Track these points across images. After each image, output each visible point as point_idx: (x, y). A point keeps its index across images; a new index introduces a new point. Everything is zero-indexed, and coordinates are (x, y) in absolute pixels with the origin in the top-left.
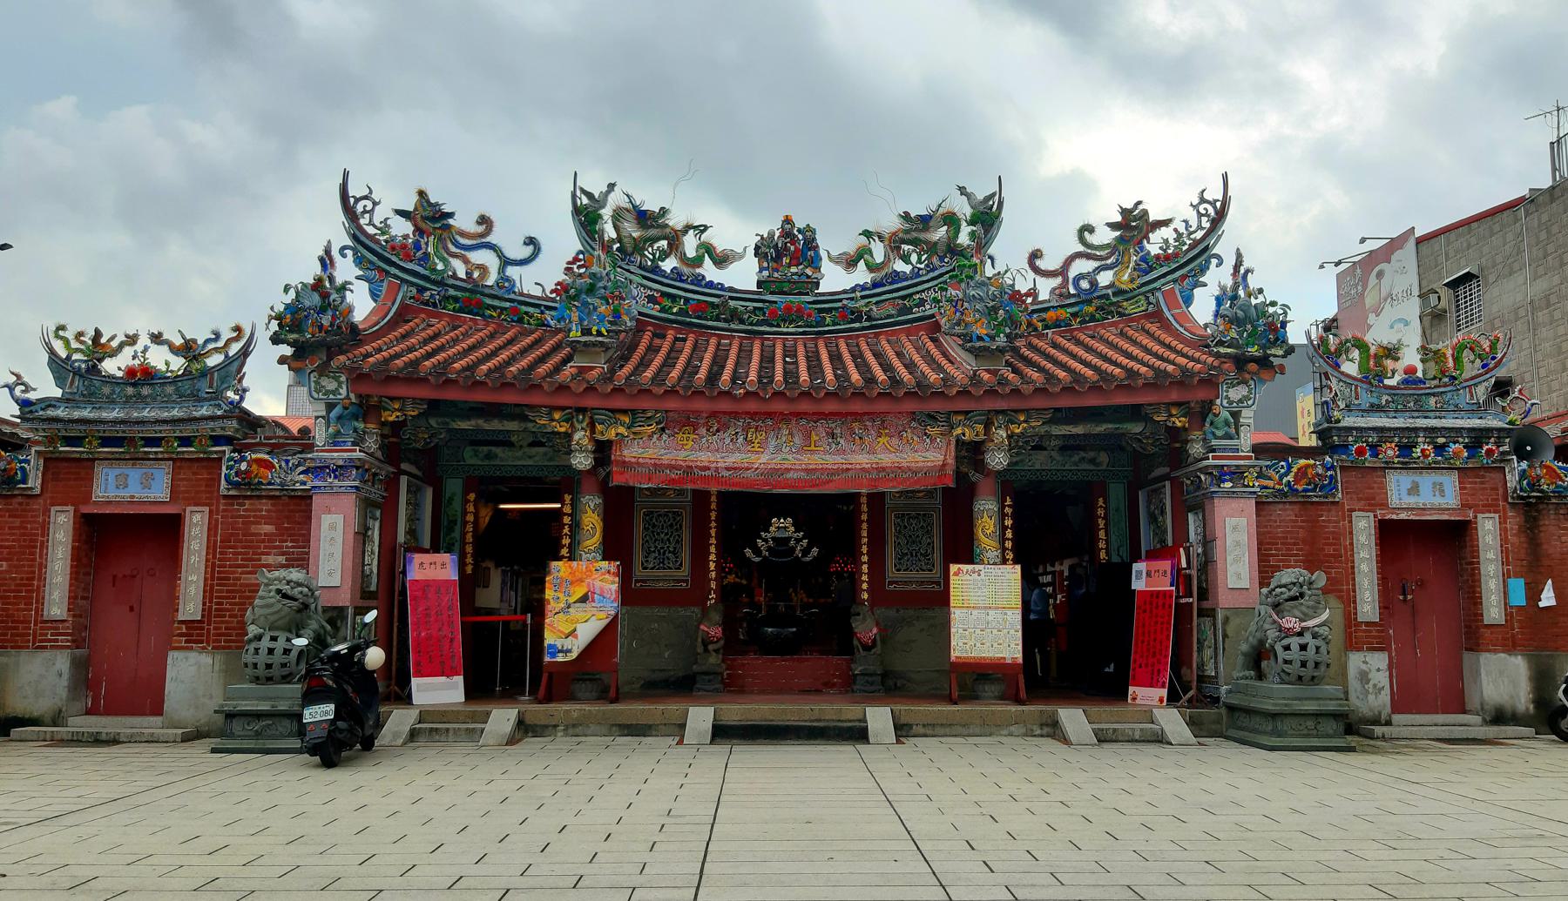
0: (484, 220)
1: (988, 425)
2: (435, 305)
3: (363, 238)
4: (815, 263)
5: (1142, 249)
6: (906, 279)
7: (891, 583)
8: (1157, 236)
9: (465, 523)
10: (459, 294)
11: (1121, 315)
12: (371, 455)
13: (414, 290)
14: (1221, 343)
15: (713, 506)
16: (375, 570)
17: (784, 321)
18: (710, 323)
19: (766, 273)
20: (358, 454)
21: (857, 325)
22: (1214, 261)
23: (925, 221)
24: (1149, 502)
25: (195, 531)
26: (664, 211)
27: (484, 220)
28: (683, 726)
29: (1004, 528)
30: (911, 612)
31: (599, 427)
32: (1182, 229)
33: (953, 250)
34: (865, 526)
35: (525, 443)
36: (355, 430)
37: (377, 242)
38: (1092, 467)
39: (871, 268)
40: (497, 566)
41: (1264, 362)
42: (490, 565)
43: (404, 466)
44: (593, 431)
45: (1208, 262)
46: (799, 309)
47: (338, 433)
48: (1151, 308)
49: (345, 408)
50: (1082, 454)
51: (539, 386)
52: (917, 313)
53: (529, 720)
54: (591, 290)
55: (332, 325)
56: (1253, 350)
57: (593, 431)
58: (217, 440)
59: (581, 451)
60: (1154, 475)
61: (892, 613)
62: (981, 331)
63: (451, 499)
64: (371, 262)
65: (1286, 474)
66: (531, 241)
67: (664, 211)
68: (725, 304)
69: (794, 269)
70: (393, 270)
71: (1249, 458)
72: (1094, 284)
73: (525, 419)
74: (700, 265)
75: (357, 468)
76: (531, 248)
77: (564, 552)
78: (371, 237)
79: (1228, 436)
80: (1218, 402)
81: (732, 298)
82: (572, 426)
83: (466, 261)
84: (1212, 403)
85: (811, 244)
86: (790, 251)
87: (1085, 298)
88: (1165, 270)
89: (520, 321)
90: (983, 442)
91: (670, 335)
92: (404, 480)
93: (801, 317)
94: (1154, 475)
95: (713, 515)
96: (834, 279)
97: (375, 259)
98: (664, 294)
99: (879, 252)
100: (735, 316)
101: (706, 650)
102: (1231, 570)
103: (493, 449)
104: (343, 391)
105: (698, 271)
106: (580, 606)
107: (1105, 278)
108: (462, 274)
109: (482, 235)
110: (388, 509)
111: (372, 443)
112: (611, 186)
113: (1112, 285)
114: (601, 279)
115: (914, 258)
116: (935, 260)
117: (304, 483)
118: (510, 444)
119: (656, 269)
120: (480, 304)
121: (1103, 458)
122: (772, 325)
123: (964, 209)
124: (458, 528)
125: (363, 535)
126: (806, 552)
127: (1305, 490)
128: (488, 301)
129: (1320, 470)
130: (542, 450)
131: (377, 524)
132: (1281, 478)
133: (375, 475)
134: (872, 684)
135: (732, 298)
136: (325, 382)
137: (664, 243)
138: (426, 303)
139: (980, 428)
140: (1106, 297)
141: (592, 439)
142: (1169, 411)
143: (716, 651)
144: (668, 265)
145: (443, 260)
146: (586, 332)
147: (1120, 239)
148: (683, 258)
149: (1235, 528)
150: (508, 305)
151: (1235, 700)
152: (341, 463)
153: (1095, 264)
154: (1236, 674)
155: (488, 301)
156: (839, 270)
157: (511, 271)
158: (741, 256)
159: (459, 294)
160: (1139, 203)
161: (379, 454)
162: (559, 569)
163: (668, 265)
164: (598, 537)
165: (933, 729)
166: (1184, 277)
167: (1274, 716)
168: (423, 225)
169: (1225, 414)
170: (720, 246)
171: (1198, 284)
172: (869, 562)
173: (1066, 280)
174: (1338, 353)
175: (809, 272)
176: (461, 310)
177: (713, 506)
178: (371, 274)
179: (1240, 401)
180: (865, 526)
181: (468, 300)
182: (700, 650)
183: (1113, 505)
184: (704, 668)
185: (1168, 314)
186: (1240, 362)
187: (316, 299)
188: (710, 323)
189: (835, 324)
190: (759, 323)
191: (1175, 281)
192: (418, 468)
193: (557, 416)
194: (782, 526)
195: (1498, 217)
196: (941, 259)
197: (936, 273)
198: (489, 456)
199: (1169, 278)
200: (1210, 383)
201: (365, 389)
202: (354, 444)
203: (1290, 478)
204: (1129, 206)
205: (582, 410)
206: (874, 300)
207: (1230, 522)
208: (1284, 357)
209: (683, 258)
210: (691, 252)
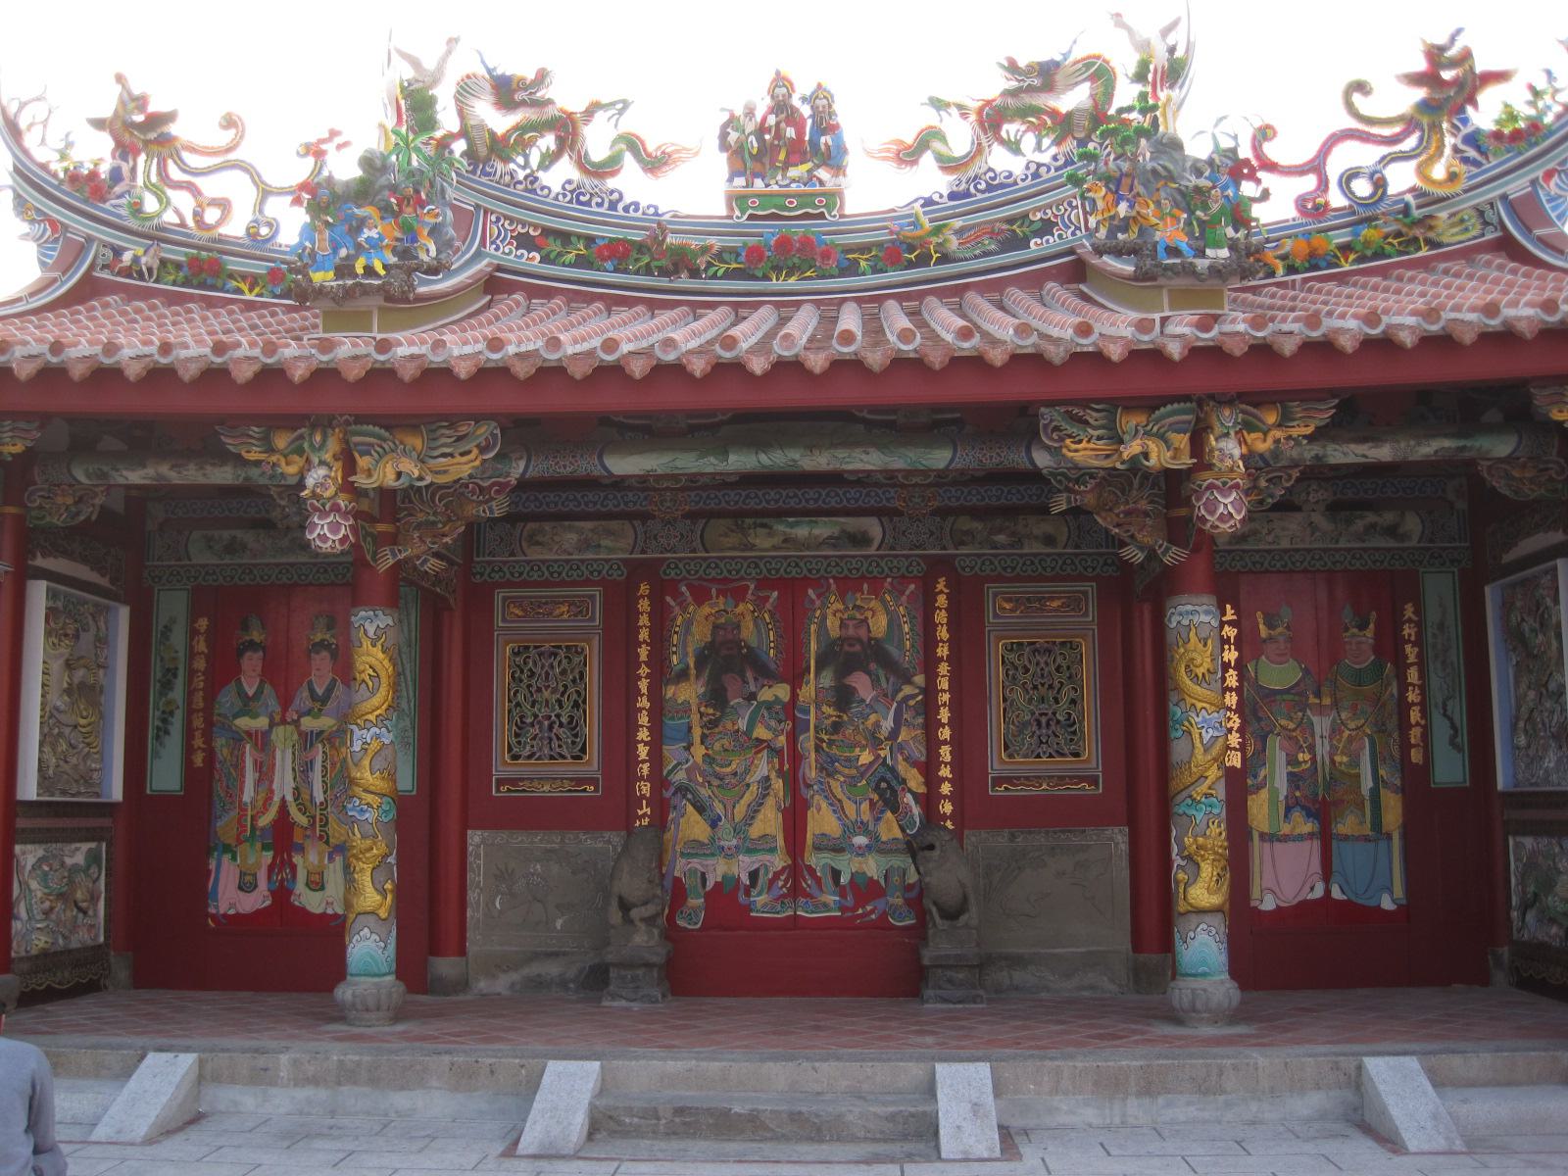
4: (834, 159)
5: (1465, 121)
7: (998, 781)
11: (1432, 244)
17: (777, 269)
23: (1047, 75)
24: (1507, 607)
26: (542, 77)
31: (363, 462)
38: (1392, 544)
39: (948, 165)
50: (1371, 517)
61: (1001, 840)
63: (167, 629)
67: (542, 77)
72: (1380, 184)
85: (825, 123)
87: (1362, 214)
98: (547, 232)
99: (960, 137)
103: (239, 534)
107: (1401, 179)
109: (229, 150)
112: (452, 42)
122: (754, 278)
123: (1124, 63)
137: (548, 141)
138: (127, 272)
139: (1182, 440)
141: (348, 487)
143: (650, 921)
147: (1425, 106)
160: (1459, 31)
168: (127, 138)
172: (953, 742)
173: (1323, 184)
182: (616, 916)
183: (1433, 615)
192: (97, 566)
193: (281, 441)
198: (232, 548)
204: (1441, 39)
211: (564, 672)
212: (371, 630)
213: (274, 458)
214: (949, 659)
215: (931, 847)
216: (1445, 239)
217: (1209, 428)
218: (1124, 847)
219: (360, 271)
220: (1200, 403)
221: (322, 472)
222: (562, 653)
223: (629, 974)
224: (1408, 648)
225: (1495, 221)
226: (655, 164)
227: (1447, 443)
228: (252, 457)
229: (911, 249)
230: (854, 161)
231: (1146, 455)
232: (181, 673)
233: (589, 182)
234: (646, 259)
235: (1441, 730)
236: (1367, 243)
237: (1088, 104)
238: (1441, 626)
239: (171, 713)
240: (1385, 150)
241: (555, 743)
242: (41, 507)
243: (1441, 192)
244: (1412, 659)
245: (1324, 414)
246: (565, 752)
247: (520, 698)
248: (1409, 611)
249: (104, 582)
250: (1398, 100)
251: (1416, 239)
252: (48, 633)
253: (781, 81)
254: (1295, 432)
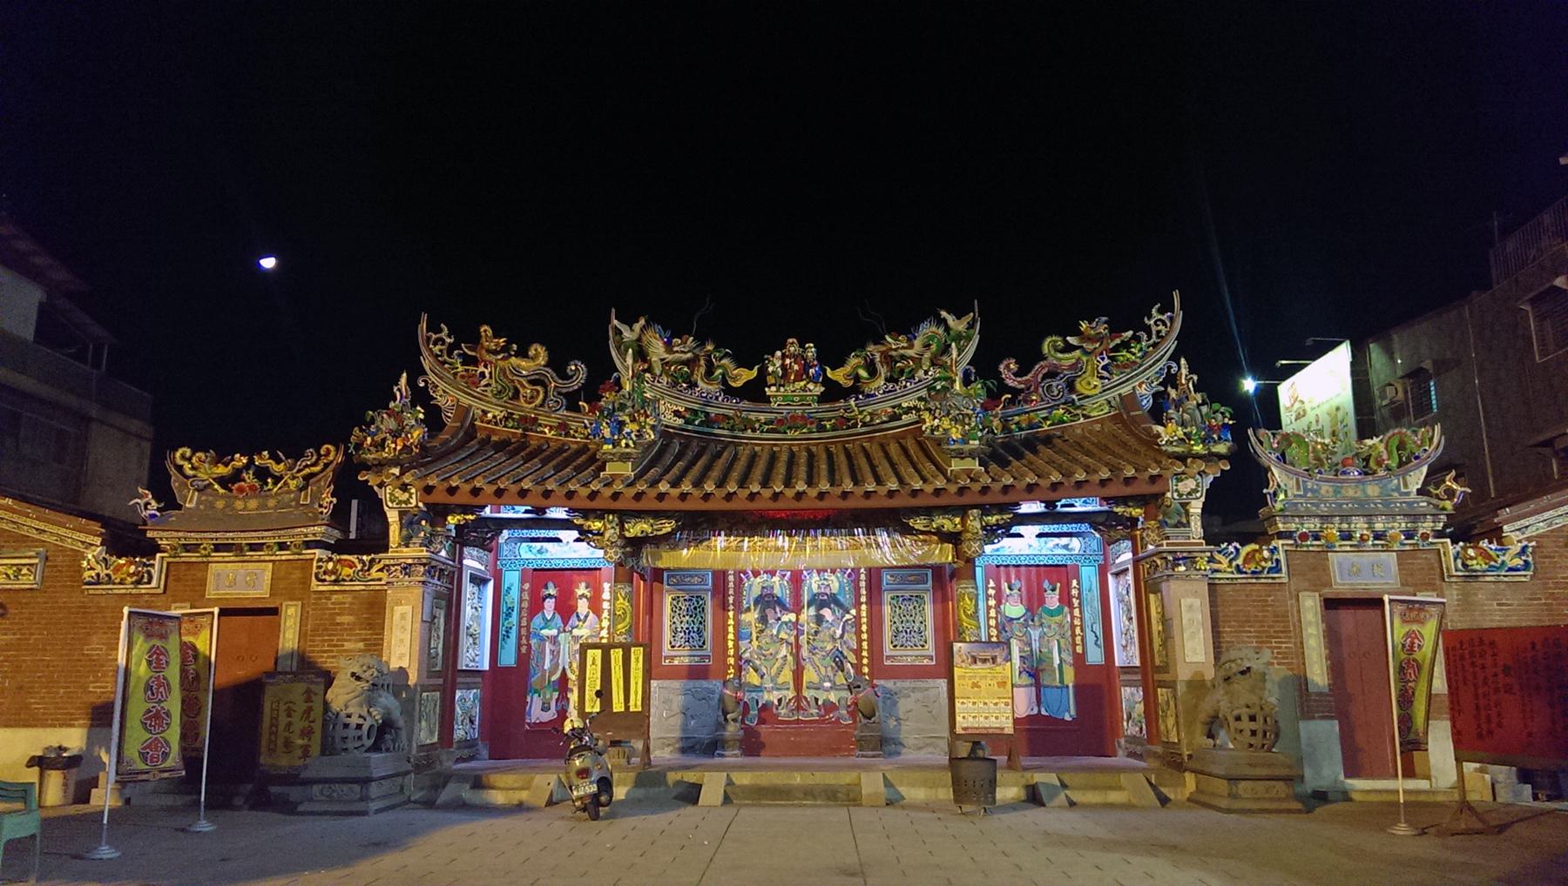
7: (888, 657)
25: (290, 622)
29: (1079, 597)
30: (458, 709)
58: (308, 545)
80: (1169, 495)
90: (960, 533)
102: (1188, 645)
104: (413, 501)
124: (515, 614)
138: (489, 422)
139: (958, 520)
143: (735, 720)
149: (1190, 607)
198: (540, 552)
203: (1240, 561)
207: (1185, 602)
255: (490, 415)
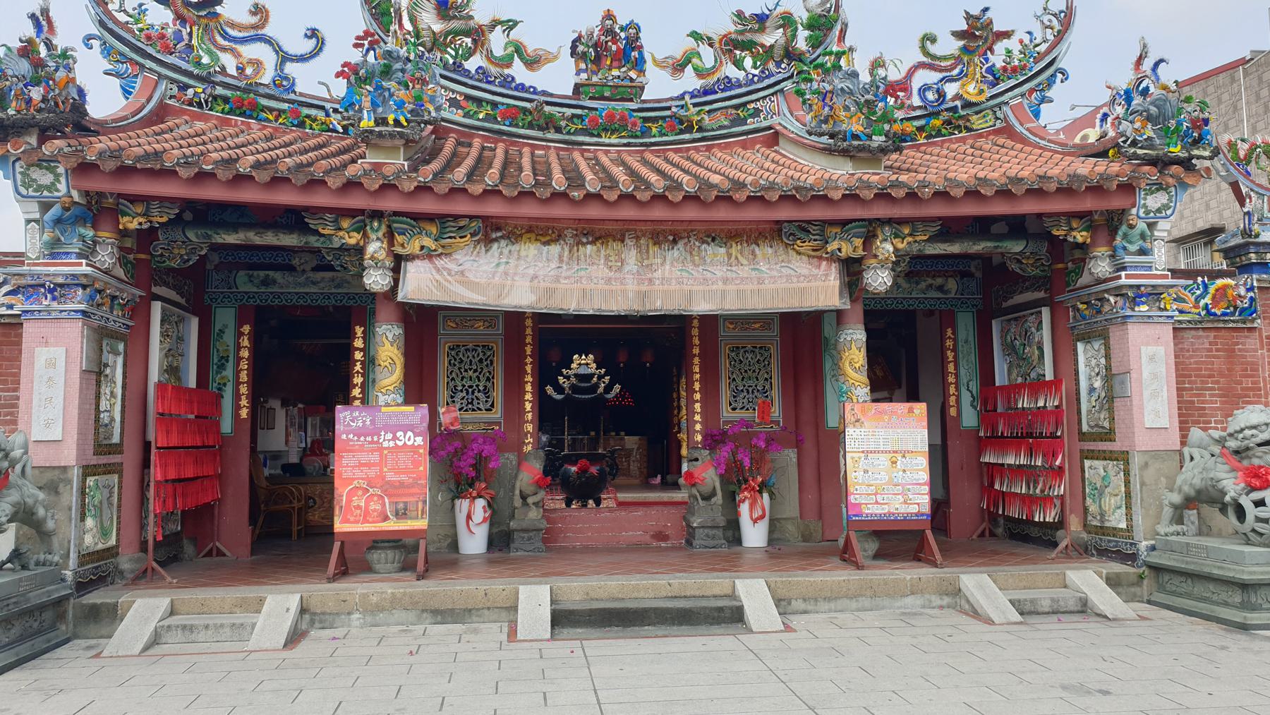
0: (258, 10)
1: (869, 239)
2: (200, 105)
3: (111, 25)
4: (639, 65)
5: (987, 60)
6: (740, 86)
8: (1000, 47)
9: (239, 359)
10: (228, 93)
11: (969, 130)
12: (106, 272)
13: (175, 89)
14: (1134, 143)
15: (529, 340)
16: (118, 417)
17: (605, 130)
18: (522, 131)
19: (584, 76)
20: (85, 269)
21: (687, 136)
22: (1059, 76)
27: (258, 10)
28: (514, 608)
31: (399, 238)
32: (1027, 40)
33: (790, 54)
34: (696, 360)
35: (308, 268)
36: (82, 238)
37: (131, 32)
38: (940, 295)
39: (700, 73)
40: (285, 404)
41: (1186, 164)
42: (275, 404)
43: (155, 290)
44: (391, 243)
45: (1053, 76)
46: (623, 118)
47: (56, 242)
48: (999, 125)
49: (66, 209)
51: (324, 183)
52: (752, 124)
53: (315, 605)
54: (387, 72)
55: (44, 100)
56: (1176, 150)
57: (391, 243)
59: (376, 267)
60: (1011, 302)
62: (857, 128)
63: (222, 331)
64: (121, 54)
65: (1202, 296)
66: (313, 33)
68: (539, 109)
69: (615, 72)
70: (149, 64)
71: (1165, 277)
72: (941, 95)
73: (304, 229)
74: (509, 65)
75: (84, 287)
76: (314, 41)
77: (356, 392)
78: (124, 26)
79: (1142, 252)
81: (548, 103)
82: (365, 236)
83: (237, 55)
84: (1123, 212)
85: (633, 43)
86: (612, 48)
88: (1012, 82)
89: (301, 125)
91: (477, 143)
92: (157, 307)
93: (624, 127)
94: (1011, 302)
95: (529, 350)
96: (659, 86)
97: (126, 50)
98: (468, 97)
99: (708, 56)
100: (549, 124)
101: (525, 503)
103: (271, 273)
104: (62, 187)
105: (506, 71)
106: (380, 449)
108: (232, 70)
109: (254, 27)
110: (136, 339)
111: (106, 257)
113: (957, 97)
114: (398, 58)
115: (748, 62)
116: (771, 66)
117: (11, 307)
118: (292, 269)
119: (457, 67)
120: (254, 106)
121: (952, 285)
122: (592, 135)
124: (230, 366)
125: (96, 374)
126: (608, 389)
127: (1224, 314)
128: (264, 102)
129: (1242, 291)
130: (328, 275)
131: (120, 360)
132: (1198, 299)
133: (114, 298)
134: (713, 538)
135: (548, 103)
136: (36, 174)
139: (858, 242)
140: (954, 109)
142: (1069, 223)
144: (472, 64)
145: (210, 53)
146: (382, 121)
147: (965, 49)
148: (490, 57)
149: (1152, 358)
150: (285, 106)
151: (1155, 559)
152: (60, 280)
153: (940, 75)
154: (1162, 529)
155: (264, 102)
156: (665, 75)
157: (290, 68)
158: (556, 58)
159: (228, 93)
160: (986, 10)
161: (120, 272)
162: (347, 419)
163: (472, 64)
164: (398, 373)
165: (814, 598)
166: (1032, 91)
167: (1244, 586)
169: (1142, 226)
170: (531, 47)
171: (1044, 100)
174: (1248, 160)
175: (633, 74)
176: (231, 112)
177: (529, 340)
178: (122, 68)
179: (1159, 210)
180: (696, 360)
181: (240, 100)
182: (518, 502)
184: (524, 525)
185: (1019, 128)
186: (1161, 163)
187: (24, 67)
188: (522, 131)
189: (662, 135)
190: (576, 133)
191: (1023, 95)
193: (345, 224)
194: (583, 364)
195: (1213, 80)
196: (778, 65)
197: (772, 80)
199: (1017, 91)
200: (1128, 188)
201: (97, 184)
202: (80, 256)
203: (1208, 300)
205: (377, 215)
206: (707, 108)
207: (1146, 351)
208: (1211, 158)
209: (490, 57)
210: (498, 51)
211: (481, 361)
212: (390, 337)
213: (341, 233)
214: (700, 355)
215: (697, 460)
216: (975, 127)
217: (875, 236)
218: (795, 460)
219: (391, 122)
220: (870, 224)
221: (378, 244)
222: (480, 350)
223: (526, 535)
224: (949, 353)
225: (1002, 116)
226: (532, 63)
227: (989, 244)
228: (325, 232)
229: (681, 123)
230: (649, 66)
231: (840, 250)
232: (231, 359)
233: (494, 70)
234: (530, 118)
235: (966, 398)
236: (933, 128)
237: (782, 41)
238: (966, 342)
239: (225, 385)
240: (940, 75)
241: (475, 402)
242: (162, 255)
243: (974, 100)
244: (951, 359)
245: (935, 228)
246: (481, 406)
247: (454, 375)
248: (949, 332)
249: (183, 301)
250: (948, 46)
251: (959, 126)
252: (162, 334)
253: (609, 16)
254: (918, 238)
255: (190, 92)
